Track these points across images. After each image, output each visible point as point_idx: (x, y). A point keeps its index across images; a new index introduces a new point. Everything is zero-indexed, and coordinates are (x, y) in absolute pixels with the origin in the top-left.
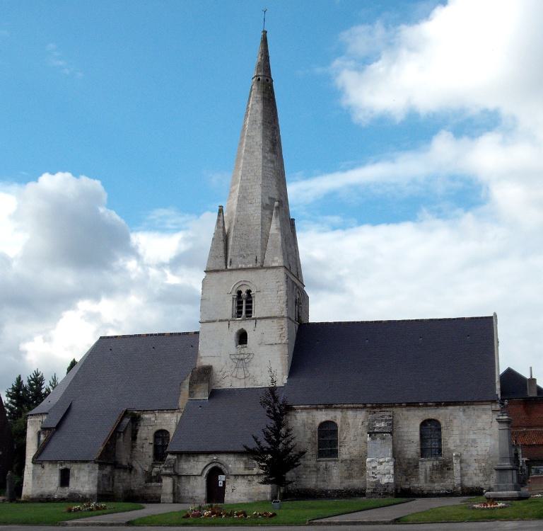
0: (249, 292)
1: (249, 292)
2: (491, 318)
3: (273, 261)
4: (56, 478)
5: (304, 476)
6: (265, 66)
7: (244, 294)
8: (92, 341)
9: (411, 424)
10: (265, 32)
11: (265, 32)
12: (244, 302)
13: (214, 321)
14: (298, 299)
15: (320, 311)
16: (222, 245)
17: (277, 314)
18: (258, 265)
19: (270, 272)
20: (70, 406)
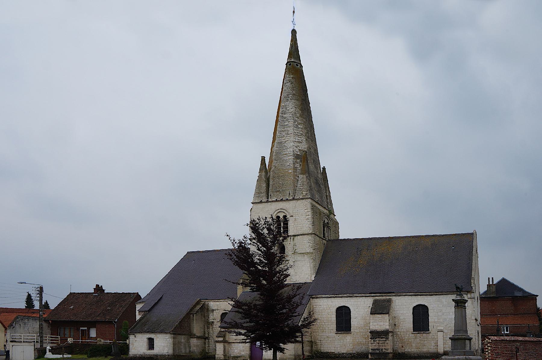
0: (285, 217)
1: (285, 217)
2: (472, 234)
3: (243, 347)
4: (156, 343)
5: (326, 344)
6: (294, 52)
7: (281, 217)
8: (182, 254)
9: (404, 306)
10: (294, 32)
11: (294, 32)
12: (282, 224)
13: (301, 253)
14: (325, 222)
15: (347, 231)
16: (264, 185)
17: (310, 232)
18: (291, 198)
19: (299, 202)
20: (161, 298)
